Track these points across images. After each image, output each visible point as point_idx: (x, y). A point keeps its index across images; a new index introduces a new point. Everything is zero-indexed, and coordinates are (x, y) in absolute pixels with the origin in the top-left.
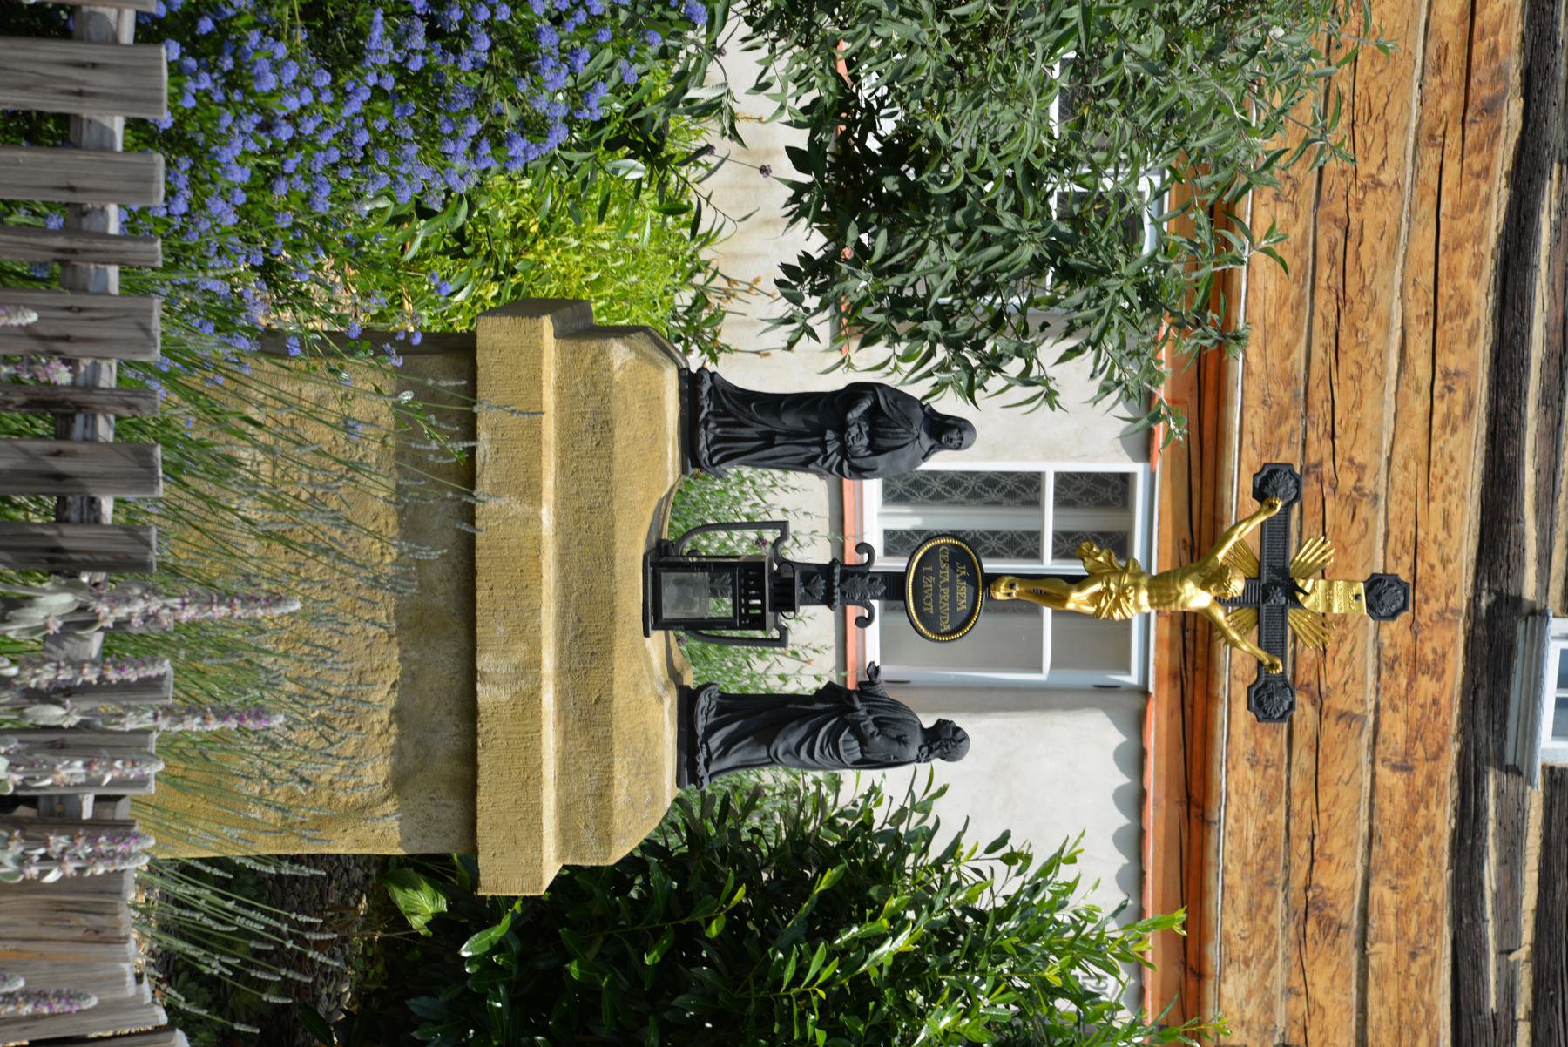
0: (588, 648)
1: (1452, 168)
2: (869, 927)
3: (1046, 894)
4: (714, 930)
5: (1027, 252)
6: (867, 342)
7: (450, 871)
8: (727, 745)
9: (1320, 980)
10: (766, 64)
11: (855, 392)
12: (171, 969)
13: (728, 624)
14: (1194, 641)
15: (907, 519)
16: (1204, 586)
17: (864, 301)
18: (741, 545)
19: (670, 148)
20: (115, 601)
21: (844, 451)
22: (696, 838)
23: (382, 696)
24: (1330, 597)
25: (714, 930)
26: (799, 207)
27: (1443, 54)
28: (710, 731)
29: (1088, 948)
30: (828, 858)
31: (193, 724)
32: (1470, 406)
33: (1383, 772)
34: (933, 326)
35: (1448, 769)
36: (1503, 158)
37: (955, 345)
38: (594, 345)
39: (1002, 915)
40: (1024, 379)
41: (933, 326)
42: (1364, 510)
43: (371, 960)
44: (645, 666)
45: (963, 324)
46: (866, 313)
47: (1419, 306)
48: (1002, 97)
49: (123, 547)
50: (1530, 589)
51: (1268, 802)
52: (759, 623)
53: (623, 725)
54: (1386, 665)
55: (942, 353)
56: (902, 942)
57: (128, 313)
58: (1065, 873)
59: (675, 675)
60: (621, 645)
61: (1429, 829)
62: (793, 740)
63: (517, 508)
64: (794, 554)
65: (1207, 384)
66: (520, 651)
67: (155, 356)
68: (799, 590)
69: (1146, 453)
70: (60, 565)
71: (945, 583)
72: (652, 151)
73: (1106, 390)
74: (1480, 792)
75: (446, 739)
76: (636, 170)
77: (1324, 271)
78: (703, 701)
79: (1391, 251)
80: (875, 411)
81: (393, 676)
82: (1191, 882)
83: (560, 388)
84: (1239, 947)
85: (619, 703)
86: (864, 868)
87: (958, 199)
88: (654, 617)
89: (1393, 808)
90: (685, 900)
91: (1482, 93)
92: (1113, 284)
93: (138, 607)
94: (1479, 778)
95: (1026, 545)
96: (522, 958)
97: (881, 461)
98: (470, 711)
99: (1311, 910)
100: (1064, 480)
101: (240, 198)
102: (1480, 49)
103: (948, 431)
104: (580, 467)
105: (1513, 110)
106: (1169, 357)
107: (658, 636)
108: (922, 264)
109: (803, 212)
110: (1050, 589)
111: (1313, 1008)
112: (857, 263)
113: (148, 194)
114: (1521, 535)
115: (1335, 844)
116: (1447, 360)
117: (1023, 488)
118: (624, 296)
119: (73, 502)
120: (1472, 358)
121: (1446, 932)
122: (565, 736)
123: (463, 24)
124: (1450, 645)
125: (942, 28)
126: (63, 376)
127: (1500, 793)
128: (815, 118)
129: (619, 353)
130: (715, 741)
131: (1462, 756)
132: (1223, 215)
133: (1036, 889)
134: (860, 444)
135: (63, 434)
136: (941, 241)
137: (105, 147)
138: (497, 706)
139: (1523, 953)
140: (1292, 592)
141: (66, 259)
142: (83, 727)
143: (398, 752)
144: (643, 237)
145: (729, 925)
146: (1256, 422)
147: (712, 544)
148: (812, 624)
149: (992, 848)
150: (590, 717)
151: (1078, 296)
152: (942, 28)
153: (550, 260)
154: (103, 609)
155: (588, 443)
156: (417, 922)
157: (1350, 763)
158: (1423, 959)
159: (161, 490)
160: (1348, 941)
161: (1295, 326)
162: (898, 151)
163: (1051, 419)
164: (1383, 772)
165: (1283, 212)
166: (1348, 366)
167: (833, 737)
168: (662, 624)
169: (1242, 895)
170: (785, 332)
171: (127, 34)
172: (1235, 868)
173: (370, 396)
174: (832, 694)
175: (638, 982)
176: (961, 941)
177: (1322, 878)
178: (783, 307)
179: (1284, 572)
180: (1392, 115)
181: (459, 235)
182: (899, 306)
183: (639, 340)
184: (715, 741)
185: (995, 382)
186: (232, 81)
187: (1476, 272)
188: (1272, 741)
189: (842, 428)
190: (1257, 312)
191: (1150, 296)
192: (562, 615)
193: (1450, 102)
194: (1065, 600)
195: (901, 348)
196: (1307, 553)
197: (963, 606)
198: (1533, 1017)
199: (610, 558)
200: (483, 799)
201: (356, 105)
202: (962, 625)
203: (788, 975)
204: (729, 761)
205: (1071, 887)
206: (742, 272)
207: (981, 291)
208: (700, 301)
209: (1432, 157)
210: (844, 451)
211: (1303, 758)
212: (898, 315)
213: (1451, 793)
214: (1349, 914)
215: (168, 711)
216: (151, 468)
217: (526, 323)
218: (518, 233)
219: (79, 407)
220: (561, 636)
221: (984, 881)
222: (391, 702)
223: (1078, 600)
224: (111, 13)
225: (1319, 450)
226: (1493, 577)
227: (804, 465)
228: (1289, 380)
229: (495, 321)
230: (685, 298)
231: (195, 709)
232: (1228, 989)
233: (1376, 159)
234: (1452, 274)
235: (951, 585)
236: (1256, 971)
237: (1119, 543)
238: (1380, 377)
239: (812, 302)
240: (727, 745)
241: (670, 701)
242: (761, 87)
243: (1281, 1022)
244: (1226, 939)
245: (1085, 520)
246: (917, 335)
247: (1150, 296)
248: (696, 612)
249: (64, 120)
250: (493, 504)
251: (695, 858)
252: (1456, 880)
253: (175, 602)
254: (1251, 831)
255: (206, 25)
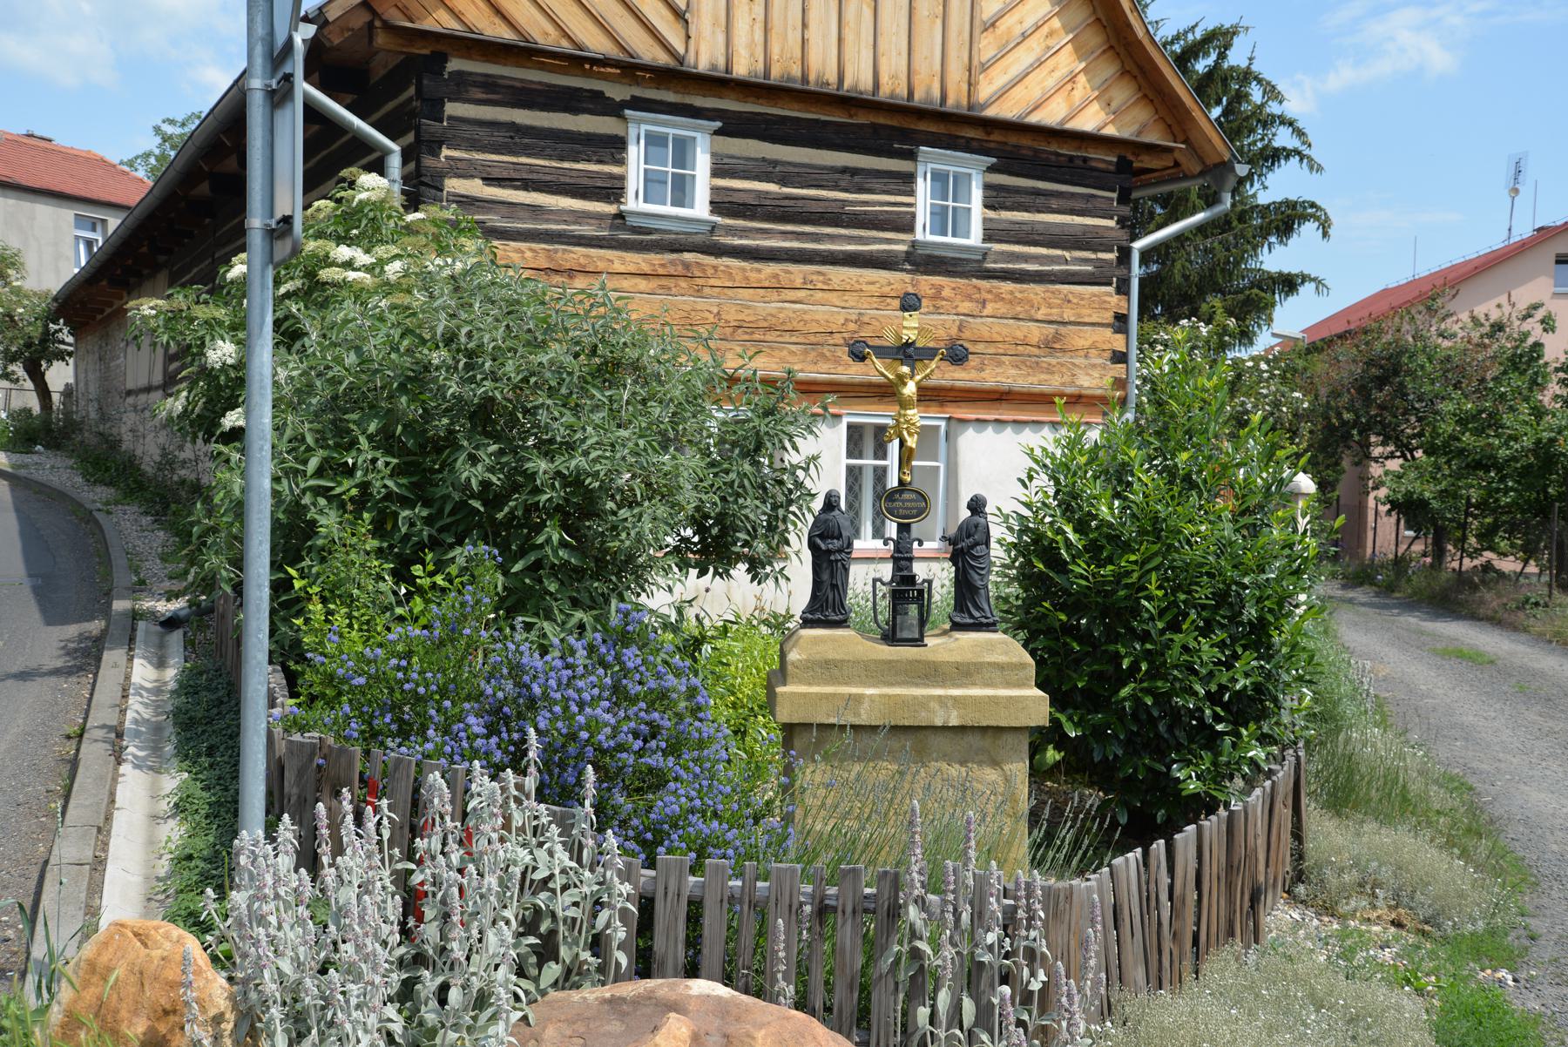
0: (932, 673)
1: (712, 282)
2: (1061, 545)
3: (1048, 462)
4: (1063, 617)
5: (747, 467)
6: (787, 543)
7: (1040, 738)
8: (979, 608)
9: (1081, 343)
10: (659, 587)
11: (812, 546)
12: (1081, 873)
13: (921, 607)
14: (929, 396)
15: (867, 528)
16: (905, 384)
17: (768, 544)
18: (884, 604)
19: (696, 633)
20: (913, 887)
21: (840, 551)
22: (1020, 626)
23: (955, 771)
24: (911, 327)
25: (1063, 617)
26: (725, 574)
27: (662, 287)
28: (972, 616)
29: (1073, 444)
30: (1029, 563)
31: (972, 853)
32: (819, 273)
33: (986, 312)
34: (781, 512)
35: (984, 284)
36: (709, 260)
37: (790, 502)
38: (789, 667)
39: (1057, 482)
40: (806, 470)
41: (781, 512)
42: (866, 319)
43: (1074, 780)
44: (942, 646)
45: (781, 498)
46: (774, 544)
47: (774, 295)
48: (677, 476)
49: (887, 885)
50: (903, 248)
51: (1000, 364)
52: (921, 592)
53: (968, 657)
54: (937, 310)
55: (793, 508)
56: (1068, 529)
57: (778, 878)
58: (1038, 453)
59: (945, 633)
60: (931, 657)
61: (1012, 293)
62: (976, 577)
63: (866, 705)
64: (887, 577)
65: (810, 389)
66: (934, 705)
67: (799, 867)
68: (905, 573)
69: (837, 417)
70: (895, 912)
71: (902, 504)
72: (698, 642)
73: (812, 432)
74: (995, 270)
75: (975, 740)
76: (707, 648)
77: (756, 337)
78: (958, 619)
79: (748, 307)
80: (821, 536)
81: (944, 766)
82: (1042, 400)
83: (810, 684)
84: (1066, 379)
85: (959, 659)
86: (1036, 548)
87: (723, 499)
88: (918, 642)
89: (1002, 309)
90: (1049, 632)
91: (680, 270)
92: (763, 429)
93: (915, 875)
94: (988, 271)
95: (881, 474)
96: (1076, 708)
97: (845, 534)
98: (962, 729)
99: (1049, 345)
100: (850, 455)
101: (725, 826)
102: (661, 271)
103: (830, 503)
104: (846, 677)
105: (687, 256)
106: (794, 405)
107: (926, 640)
108: (752, 516)
109: (727, 572)
110: (906, 456)
111: (1093, 346)
112: (750, 547)
113: (724, 867)
114: (878, 251)
115: (1019, 334)
116: (798, 282)
117: (853, 474)
118: (763, 657)
119: (864, 907)
120: (798, 271)
121: (1058, 287)
122: (974, 684)
123: (646, 724)
124: (926, 283)
125: (646, 504)
126: (808, 909)
127: (995, 262)
128: (684, 565)
129: (793, 656)
130: (977, 614)
131: (978, 277)
132: (733, 380)
133: (1045, 466)
134: (836, 544)
135: (835, 909)
136: (742, 507)
137: (703, 885)
138: (960, 716)
139: (1067, 255)
140: (908, 345)
141: (753, 905)
142: (972, 904)
143: (980, 763)
144: (737, 647)
145: (1062, 610)
146: (825, 367)
147: (884, 615)
148: (920, 570)
149: (1025, 486)
150: (965, 672)
151: (769, 445)
152: (646, 504)
153: (747, 691)
154: (916, 892)
155: (836, 671)
156: (1058, 757)
157: (981, 327)
158: (1070, 297)
159: (861, 866)
160: (1063, 330)
161: (781, 349)
162: (701, 530)
163: (822, 457)
164: (986, 312)
165: (729, 355)
166: (800, 326)
167: (975, 558)
168: (921, 638)
169: (1043, 376)
170: (782, 581)
171: (652, 873)
172: (1030, 379)
173: (812, 774)
174: (954, 559)
175: (1087, 653)
176: (1069, 502)
177: (1034, 341)
178: (770, 582)
179: (899, 348)
180: (687, 308)
181: (735, 733)
182: (771, 528)
183: (787, 647)
184: (977, 614)
185: (808, 483)
186: (675, 826)
187: (759, 271)
188: (973, 361)
189: (829, 552)
190: (774, 366)
191: (768, 413)
192: (917, 685)
193: (683, 283)
194: (911, 449)
195: (791, 528)
196: (890, 340)
197: (913, 496)
198: (1095, 251)
199: (890, 662)
200: (1003, 724)
201: (682, 772)
202: (922, 497)
203: (1084, 583)
204: (986, 607)
205: (1044, 449)
206: (752, 603)
207: (765, 489)
208: (765, 622)
209: (707, 290)
210: (840, 551)
211: (980, 348)
212: (775, 529)
213: (995, 283)
214: (1051, 329)
215: (965, 865)
216: (850, 871)
217: (779, 699)
218: (734, 705)
219: (822, 901)
220: (927, 686)
221: (1041, 489)
222: (957, 766)
223: (911, 442)
224: (643, 879)
225: (838, 339)
226: (897, 263)
227: (846, 570)
228: (806, 352)
229: (778, 714)
230: (764, 629)
231: (965, 852)
232: (1086, 384)
233: (707, 315)
234: (760, 281)
235: (903, 501)
236: (1077, 371)
237: (880, 430)
238: (805, 312)
239: (768, 569)
240: (979, 608)
241: (957, 635)
242: (670, 590)
243: (1100, 361)
244: (1063, 384)
245: (869, 444)
246: (785, 520)
247: (768, 413)
248: (915, 622)
249: (690, 903)
250: (864, 716)
251: (1031, 627)
252: (1034, 282)
253: (913, 859)
254: (1013, 372)
255: (649, 836)
